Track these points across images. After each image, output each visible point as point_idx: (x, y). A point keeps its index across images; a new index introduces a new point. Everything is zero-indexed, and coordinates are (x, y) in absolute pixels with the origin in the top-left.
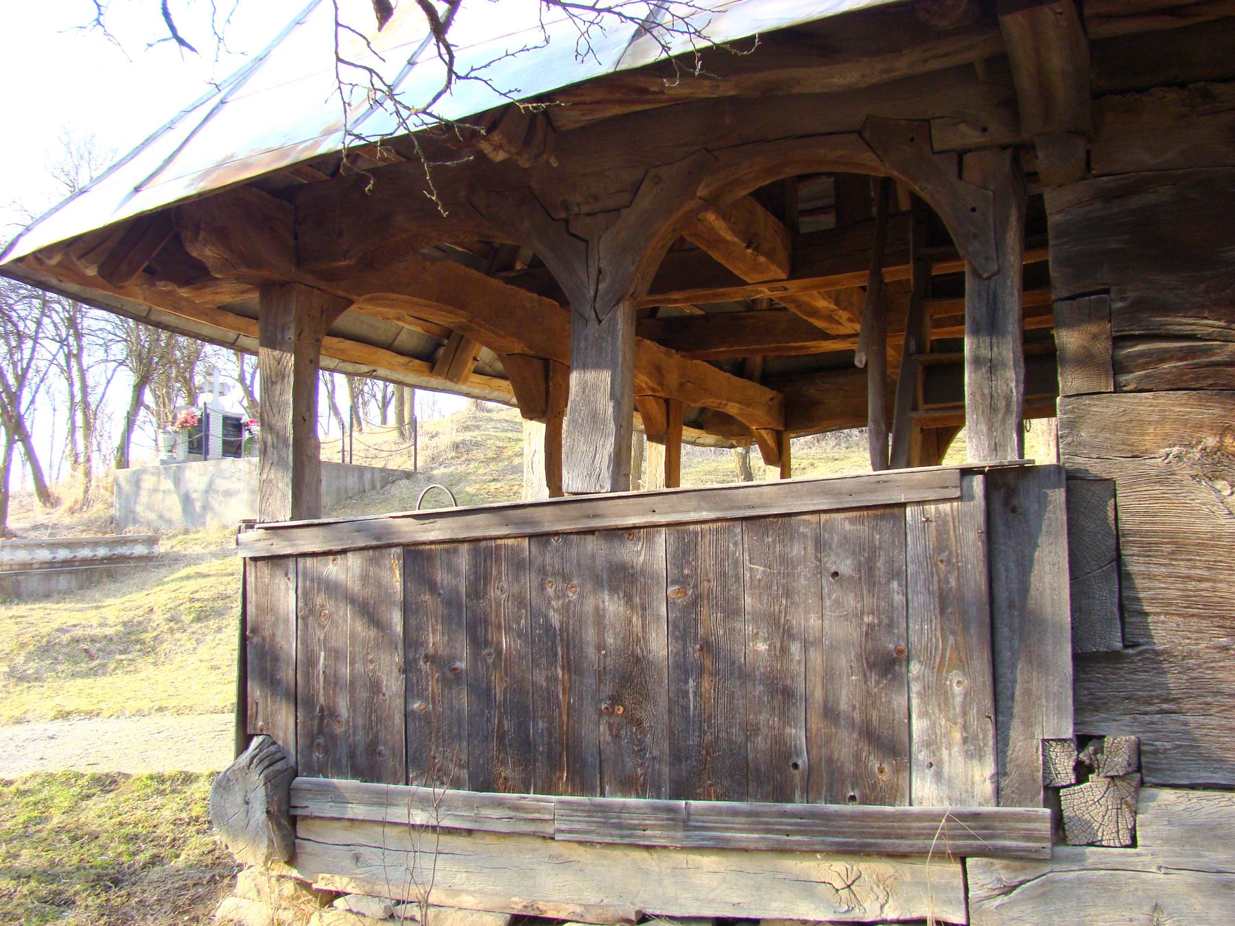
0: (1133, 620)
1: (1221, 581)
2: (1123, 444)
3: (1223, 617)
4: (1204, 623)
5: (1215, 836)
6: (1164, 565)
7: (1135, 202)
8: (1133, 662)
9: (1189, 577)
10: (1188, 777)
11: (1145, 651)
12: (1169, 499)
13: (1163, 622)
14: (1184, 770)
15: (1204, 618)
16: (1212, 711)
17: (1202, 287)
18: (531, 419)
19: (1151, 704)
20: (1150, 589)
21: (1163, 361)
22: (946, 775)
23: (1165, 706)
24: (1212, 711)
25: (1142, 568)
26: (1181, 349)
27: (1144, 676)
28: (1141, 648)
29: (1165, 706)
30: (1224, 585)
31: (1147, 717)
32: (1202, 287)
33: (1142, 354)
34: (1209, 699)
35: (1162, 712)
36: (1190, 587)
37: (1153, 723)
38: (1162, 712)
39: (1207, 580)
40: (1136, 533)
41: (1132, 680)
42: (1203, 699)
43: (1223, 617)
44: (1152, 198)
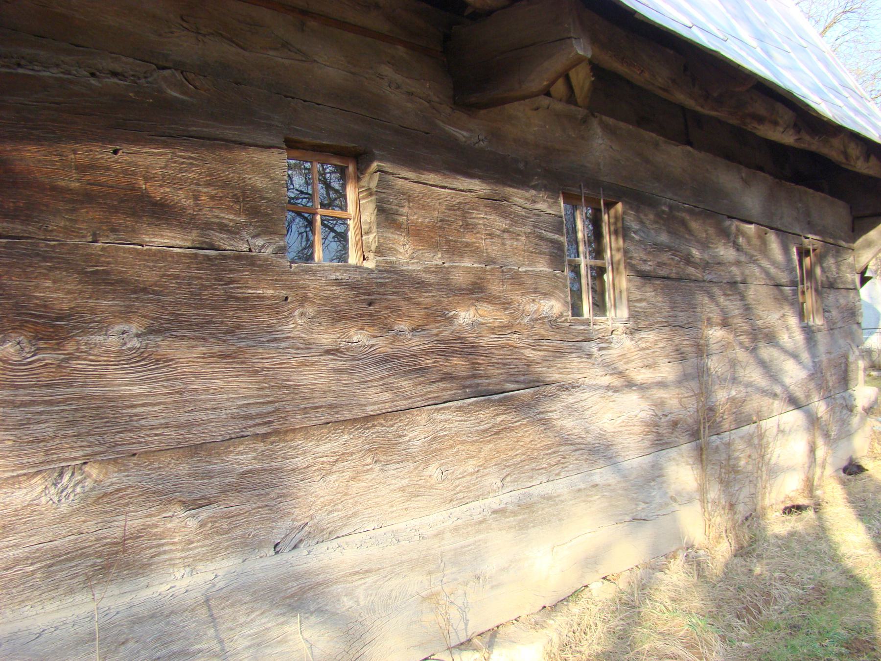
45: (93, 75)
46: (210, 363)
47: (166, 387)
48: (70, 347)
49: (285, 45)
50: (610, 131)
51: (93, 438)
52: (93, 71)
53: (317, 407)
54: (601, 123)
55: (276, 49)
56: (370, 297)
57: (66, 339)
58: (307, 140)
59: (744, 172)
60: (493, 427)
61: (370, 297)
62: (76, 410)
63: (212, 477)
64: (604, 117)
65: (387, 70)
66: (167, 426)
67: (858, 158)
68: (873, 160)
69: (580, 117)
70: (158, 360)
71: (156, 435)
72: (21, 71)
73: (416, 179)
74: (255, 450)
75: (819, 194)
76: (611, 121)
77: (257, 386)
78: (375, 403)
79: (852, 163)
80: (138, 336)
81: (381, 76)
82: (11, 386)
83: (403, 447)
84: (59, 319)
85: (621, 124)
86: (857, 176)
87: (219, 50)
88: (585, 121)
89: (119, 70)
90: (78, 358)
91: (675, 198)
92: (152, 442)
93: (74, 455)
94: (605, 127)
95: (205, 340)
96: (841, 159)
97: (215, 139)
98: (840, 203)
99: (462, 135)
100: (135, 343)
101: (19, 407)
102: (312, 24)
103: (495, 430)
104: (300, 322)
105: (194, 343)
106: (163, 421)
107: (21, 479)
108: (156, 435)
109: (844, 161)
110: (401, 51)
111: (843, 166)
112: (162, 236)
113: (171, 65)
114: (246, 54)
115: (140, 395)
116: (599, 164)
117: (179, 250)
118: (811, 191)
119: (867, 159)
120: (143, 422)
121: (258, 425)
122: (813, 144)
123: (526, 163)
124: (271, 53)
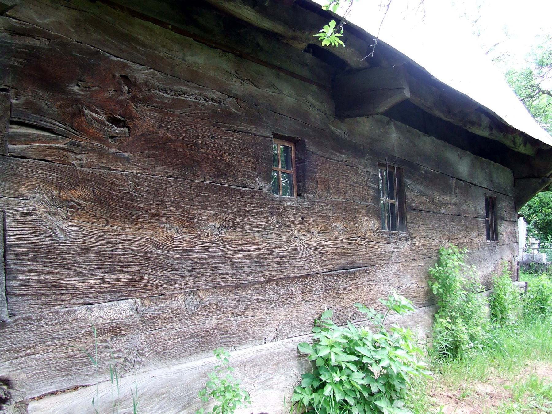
0: (12, 300)
1: (56, 273)
2: (10, 189)
3: (56, 294)
4: (48, 298)
5: (358, 356)
6: (29, 265)
7: (28, 41)
8: (11, 327)
9: (43, 272)
10: (39, 392)
11: (18, 319)
12: (33, 225)
13: (28, 300)
14: (37, 388)
15: (47, 295)
16: (51, 350)
17: (59, 103)
18: (245, 5)
19: (21, 352)
20: (21, 280)
21: (34, 141)
22: (356, 338)
23: (28, 351)
24: (50, 350)
25: (17, 268)
26: (44, 136)
27: (17, 335)
28: (17, 317)
29: (28, 351)
30: (57, 276)
31: (18, 360)
32: (59, 103)
33: (25, 135)
34: (50, 343)
35: (27, 355)
36: (42, 278)
37: (21, 363)
38: (27, 355)
39: (51, 273)
40: (15, 245)
41: (10, 339)
42: (47, 344)
43: (56, 294)
44: (36, 42)
45: (205, 100)
46: (243, 244)
47: (228, 254)
48: (194, 233)
49: (273, 86)
50: (398, 128)
51: (200, 278)
52: (205, 98)
53: (282, 270)
54: (395, 124)
55: (269, 87)
56: (303, 215)
57: (193, 228)
58: (280, 134)
59: (460, 151)
60: (349, 286)
61: (303, 215)
62: (195, 263)
63: (243, 301)
64: (396, 122)
65: (310, 98)
66: (227, 274)
67: (520, 144)
68: (528, 145)
69: (386, 121)
70: (225, 241)
71: (224, 278)
72: (180, 97)
73: (321, 155)
74: (258, 289)
75: (497, 165)
76: (399, 123)
77: (260, 256)
78: (304, 270)
79: (517, 147)
80: (218, 228)
81: (308, 101)
82: (173, 250)
83: (313, 293)
84: (191, 218)
85: (404, 125)
86: (518, 154)
87: (249, 88)
88: (388, 124)
89: (215, 98)
90: (197, 238)
91: (428, 166)
92: (222, 282)
93: (194, 286)
94: (396, 126)
95: (242, 232)
96: (512, 145)
97: (247, 133)
98: (508, 170)
99: (338, 131)
100: (217, 232)
101: (175, 260)
102: (282, 74)
103: (350, 288)
104: (277, 226)
105: (238, 233)
106: (226, 271)
107: (175, 295)
108: (224, 278)
109: (513, 146)
110: (314, 88)
111: (512, 149)
112: (228, 180)
113: (232, 95)
114: (258, 89)
115: (218, 257)
116: (393, 147)
117: (234, 187)
118: (493, 162)
119: (525, 145)
120: (219, 271)
121: (260, 276)
122: (498, 136)
123: (364, 146)
124: (267, 89)
